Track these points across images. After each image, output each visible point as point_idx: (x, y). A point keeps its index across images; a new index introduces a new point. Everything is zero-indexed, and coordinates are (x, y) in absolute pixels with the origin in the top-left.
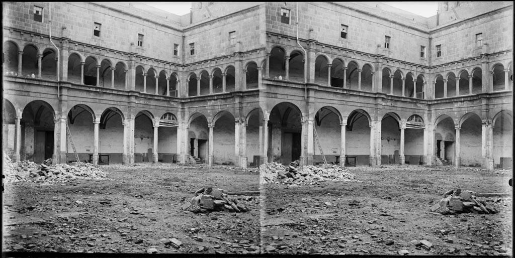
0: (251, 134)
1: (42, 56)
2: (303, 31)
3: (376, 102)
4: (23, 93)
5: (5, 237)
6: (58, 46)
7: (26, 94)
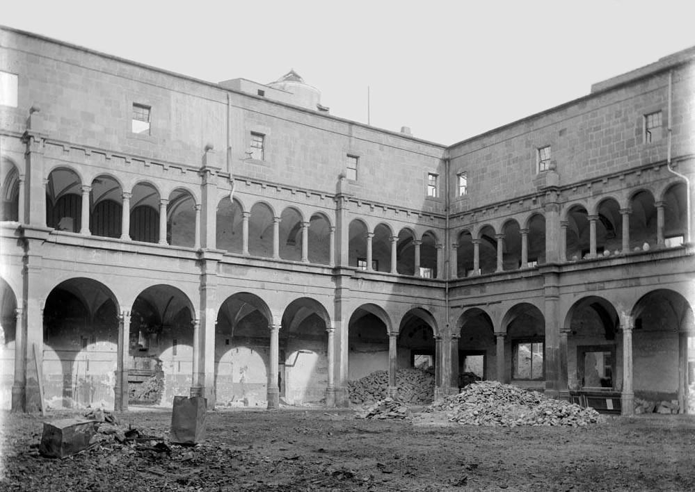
0: (357, 356)
3: (559, 282)
4: (628, 283)
7: (633, 283)
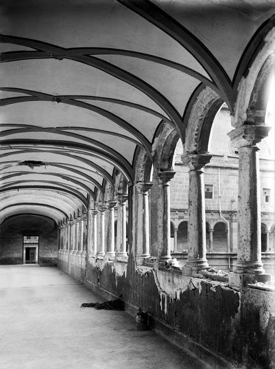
1: (213, 231)
2: (225, 202)
6: (227, 219)
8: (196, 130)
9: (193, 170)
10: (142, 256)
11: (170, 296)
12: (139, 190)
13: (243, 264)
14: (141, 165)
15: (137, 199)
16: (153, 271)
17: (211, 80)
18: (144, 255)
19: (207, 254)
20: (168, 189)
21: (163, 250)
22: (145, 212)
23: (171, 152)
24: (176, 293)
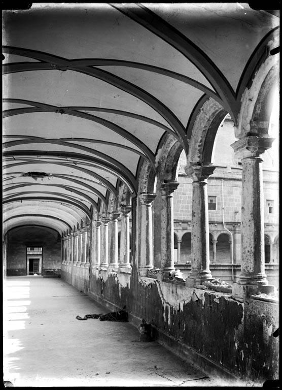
1: (217, 242)
2: (229, 214)
5: (4, 174)
6: (230, 230)
8: (199, 141)
9: (197, 182)
10: (145, 267)
11: (174, 307)
12: (142, 202)
13: (246, 275)
14: (145, 176)
15: (141, 211)
16: (157, 282)
17: (214, 91)
18: (148, 266)
19: (210, 266)
20: (172, 200)
21: (167, 261)
22: (148, 224)
23: (175, 163)
24: (179, 304)
